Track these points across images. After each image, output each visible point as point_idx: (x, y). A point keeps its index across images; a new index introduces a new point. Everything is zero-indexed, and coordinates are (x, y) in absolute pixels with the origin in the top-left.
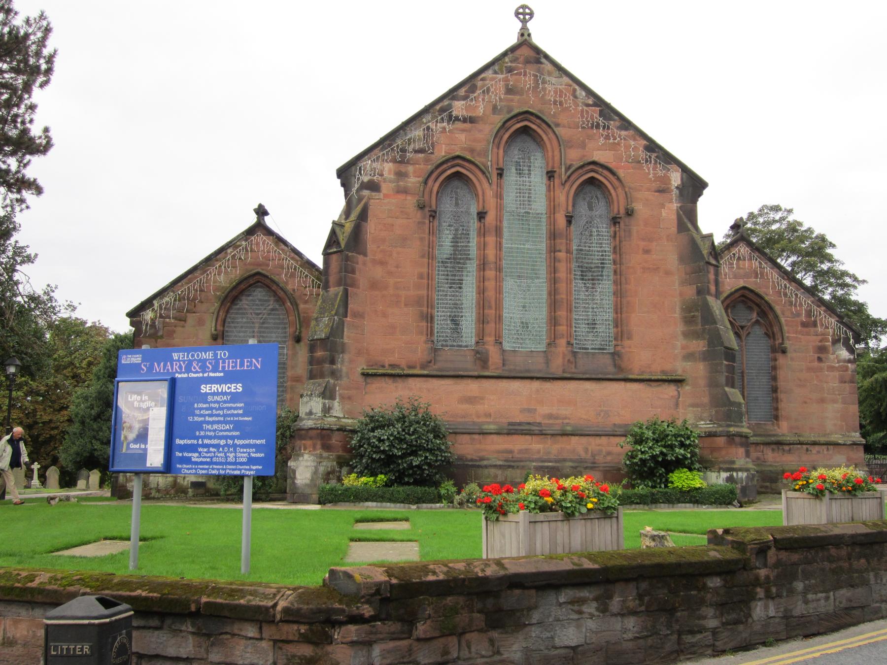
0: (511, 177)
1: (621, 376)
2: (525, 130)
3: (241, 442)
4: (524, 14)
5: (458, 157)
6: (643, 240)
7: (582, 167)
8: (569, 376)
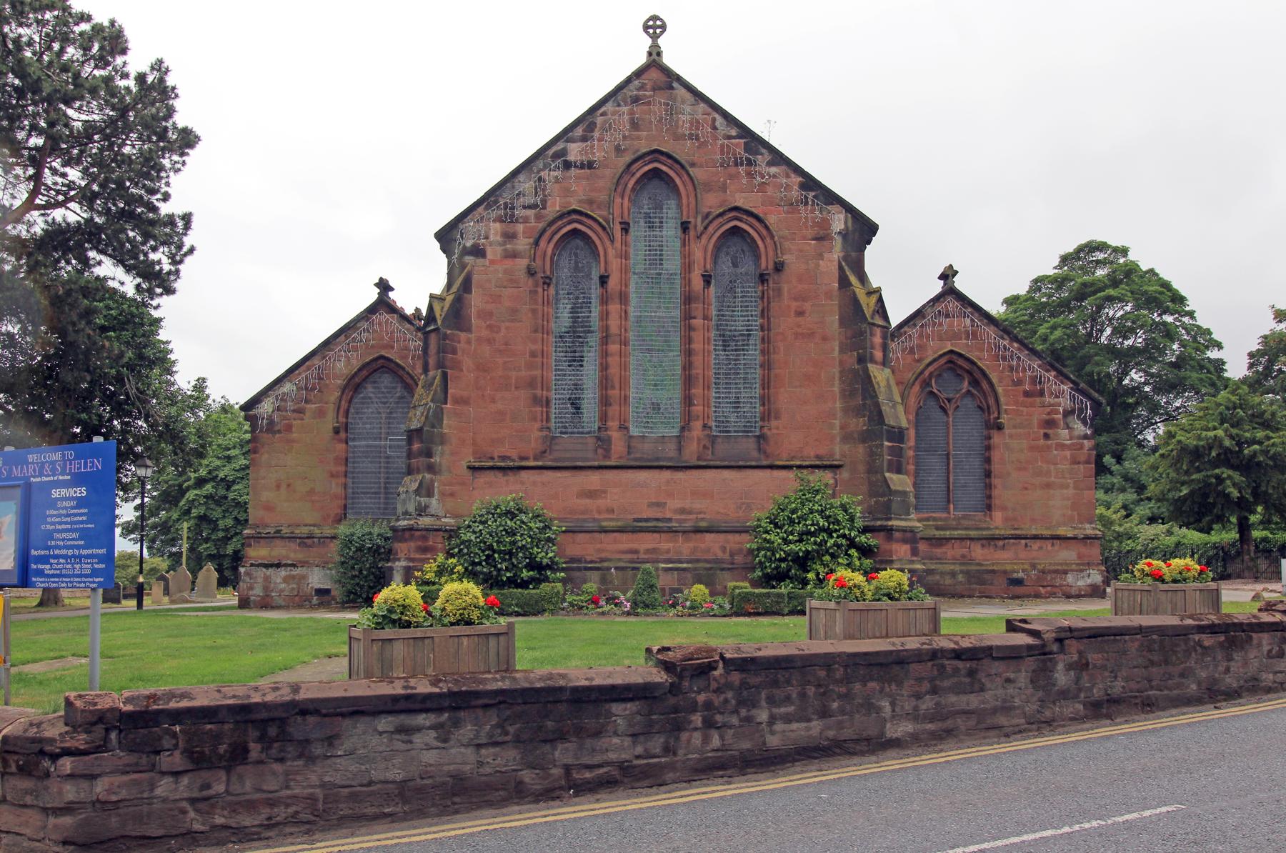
0: (638, 230)
1: (765, 463)
2: (656, 174)
3: (84, 552)
4: (654, 27)
5: (575, 211)
6: (796, 299)
7: (721, 215)
8: (704, 463)
